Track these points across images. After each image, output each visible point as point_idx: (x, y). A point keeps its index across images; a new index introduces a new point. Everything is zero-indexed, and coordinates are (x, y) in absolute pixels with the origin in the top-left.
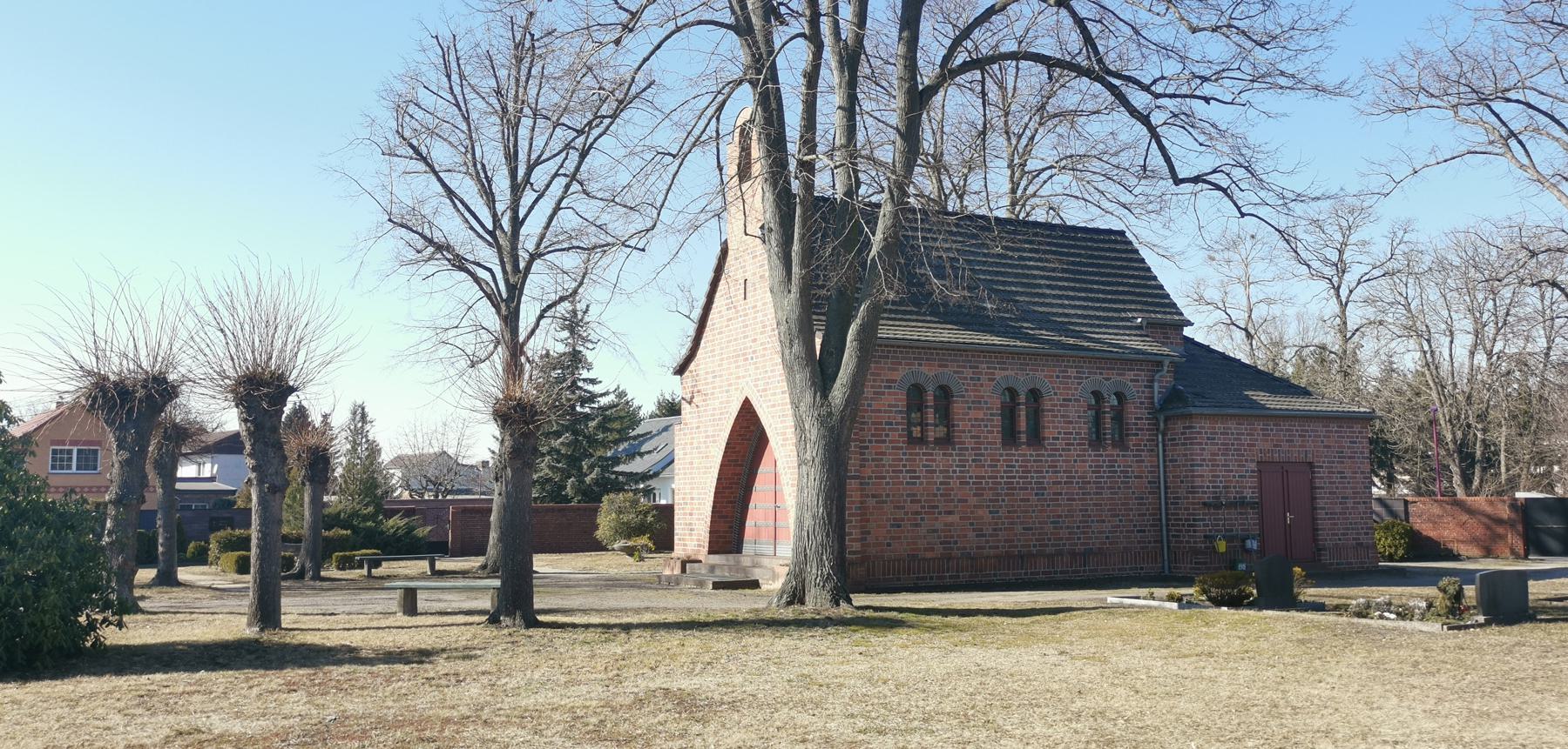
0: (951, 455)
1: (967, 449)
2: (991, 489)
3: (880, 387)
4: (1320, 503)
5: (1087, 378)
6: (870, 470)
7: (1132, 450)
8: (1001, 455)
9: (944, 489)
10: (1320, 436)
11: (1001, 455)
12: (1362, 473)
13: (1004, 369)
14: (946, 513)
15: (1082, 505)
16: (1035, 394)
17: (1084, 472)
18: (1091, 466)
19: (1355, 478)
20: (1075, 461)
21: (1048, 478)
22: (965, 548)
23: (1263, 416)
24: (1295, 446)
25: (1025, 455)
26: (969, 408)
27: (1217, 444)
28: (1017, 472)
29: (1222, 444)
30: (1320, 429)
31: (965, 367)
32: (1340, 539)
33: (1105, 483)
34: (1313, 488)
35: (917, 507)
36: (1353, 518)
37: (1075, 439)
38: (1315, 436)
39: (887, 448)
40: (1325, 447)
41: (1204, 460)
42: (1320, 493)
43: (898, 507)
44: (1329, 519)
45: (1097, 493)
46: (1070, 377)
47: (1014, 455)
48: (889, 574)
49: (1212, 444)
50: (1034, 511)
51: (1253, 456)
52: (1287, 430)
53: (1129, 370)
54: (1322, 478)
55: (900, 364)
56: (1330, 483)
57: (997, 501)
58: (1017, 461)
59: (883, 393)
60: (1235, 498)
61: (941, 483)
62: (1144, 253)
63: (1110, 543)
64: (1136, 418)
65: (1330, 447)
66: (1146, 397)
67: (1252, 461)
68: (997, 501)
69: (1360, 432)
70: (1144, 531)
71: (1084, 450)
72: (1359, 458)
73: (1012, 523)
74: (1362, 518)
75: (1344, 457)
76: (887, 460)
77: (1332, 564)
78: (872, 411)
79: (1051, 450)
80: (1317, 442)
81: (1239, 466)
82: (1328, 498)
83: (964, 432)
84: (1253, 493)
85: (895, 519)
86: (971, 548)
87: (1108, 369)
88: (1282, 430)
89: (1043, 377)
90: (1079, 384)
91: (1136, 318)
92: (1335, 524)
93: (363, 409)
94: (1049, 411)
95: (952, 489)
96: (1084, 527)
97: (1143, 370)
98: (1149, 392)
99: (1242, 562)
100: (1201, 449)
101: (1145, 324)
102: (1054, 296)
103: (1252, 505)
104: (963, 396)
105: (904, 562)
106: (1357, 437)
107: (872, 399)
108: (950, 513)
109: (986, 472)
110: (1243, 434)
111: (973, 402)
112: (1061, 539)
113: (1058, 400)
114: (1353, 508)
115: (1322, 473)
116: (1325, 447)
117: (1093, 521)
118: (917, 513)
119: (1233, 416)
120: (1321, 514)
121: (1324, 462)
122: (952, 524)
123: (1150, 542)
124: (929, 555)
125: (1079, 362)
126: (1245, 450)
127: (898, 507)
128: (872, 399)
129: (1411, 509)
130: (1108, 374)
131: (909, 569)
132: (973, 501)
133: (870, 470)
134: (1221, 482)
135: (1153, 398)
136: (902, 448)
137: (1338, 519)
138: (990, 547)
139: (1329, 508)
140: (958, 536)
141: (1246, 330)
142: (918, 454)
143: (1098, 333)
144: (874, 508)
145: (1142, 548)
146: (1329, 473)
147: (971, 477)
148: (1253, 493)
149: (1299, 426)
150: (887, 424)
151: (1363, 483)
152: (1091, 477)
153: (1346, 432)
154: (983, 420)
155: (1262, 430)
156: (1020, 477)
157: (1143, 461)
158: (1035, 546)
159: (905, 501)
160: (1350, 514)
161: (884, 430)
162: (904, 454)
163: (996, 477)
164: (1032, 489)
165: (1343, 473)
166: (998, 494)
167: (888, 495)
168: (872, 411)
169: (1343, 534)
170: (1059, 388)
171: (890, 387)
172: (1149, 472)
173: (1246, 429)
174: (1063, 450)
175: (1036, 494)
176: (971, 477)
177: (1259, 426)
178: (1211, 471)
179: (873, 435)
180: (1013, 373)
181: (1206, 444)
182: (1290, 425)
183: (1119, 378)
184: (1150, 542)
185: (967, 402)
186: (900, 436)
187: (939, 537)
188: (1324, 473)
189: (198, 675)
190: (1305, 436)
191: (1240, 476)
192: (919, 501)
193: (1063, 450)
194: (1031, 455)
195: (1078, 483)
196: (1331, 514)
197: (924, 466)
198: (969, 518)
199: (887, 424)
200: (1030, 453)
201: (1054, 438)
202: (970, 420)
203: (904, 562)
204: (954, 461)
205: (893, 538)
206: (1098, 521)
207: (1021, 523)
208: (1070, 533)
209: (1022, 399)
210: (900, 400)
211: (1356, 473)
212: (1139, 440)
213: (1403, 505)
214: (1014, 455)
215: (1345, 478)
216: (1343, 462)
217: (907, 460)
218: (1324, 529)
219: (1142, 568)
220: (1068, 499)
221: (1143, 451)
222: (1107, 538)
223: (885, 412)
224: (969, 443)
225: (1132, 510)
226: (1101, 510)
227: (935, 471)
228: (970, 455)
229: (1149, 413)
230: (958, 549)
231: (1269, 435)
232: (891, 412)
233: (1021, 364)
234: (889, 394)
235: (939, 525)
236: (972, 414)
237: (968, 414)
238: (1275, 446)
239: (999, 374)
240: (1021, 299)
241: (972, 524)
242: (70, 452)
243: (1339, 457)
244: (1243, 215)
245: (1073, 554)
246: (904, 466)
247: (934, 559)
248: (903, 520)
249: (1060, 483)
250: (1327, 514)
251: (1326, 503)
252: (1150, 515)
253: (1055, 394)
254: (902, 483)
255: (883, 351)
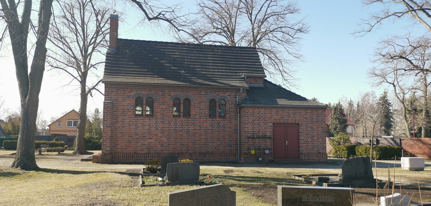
0: (152, 120)
1: (159, 118)
2: (167, 131)
3: (125, 98)
4: (301, 138)
5: (209, 95)
6: (120, 124)
7: (227, 119)
8: (172, 120)
9: (148, 131)
11: (172, 120)
13: (175, 92)
14: (149, 139)
15: (205, 137)
18: (209, 124)
20: (203, 122)
21: (191, 128)
22: (156, 150)
23: (276, 107)
24: (291, 118)
26: (160, 105)
27: (255, 117)
28: (179, 126)
30: (303, 112)
31: (159, 91)
32: (310, 151)
34: (299, 132)
35: (138, 137)
37: (203, 115)
39: (127, 117)
41: (249, 122)
43: (130, 137)
46: (202, 94)
47: (178, 120)
48: (125, 158)
49: (253, 117)
50: (185, 139)
51: (271, 121)
53: (227, 92)
55: (133, 90)
58: (179, 122)
59: (126, 100)
60: (262, 135)
61: (147, 129)
62: (28, 37)
63: (217, 150)
64: (229, 108)
65: (307, 118)
66: (234, 101)
67: (270, 123)
70: (232, 146)
71: (207, 119)
73: (176, 143)
74: (321, 143)
76: (127, 121)
78: (121, 106)
79: (193, 118)
82: (305, 136)
83: (158, 112)
84: (270, 134)
85: (128, 141)
86: (159, 150)
87: (218, 91)
89: (191, 95)
90: (206, 97)
91: (243, 75)
93: (98, 110)
94: (193, 105)
95: (152, 131)
96: (205, 144)
97: (233, 92)
98: (235, 99)
99: (260, 158)
100: (248, 118)
101: (245, 77)
102: (213, 69)
103: (270, 138)
104: (158, 101)
105: (131, 154)
107: (121, 102)
108: (151, 139)
109: (166, 125)
110: (267, 113)
111: (162, 103)
112: (196, 148)
113: (197, 102)
117: (209, 143)
118: (137, 139)
119: (262, 107)
120: (301, 142)
122: (151, 142)
123: (233, 150)
124: (142, 152)
125: (206, 89)
127: (130, 137)
128: (121, 102)
129: (402, 142)
130: (218, 93)
131: (133, 157)
132: (160, 135)
133: (120, 124)
134: (256, 130)
135: (236, 101)
136: (132, 118)
138: (166, 150)
139: (305, 140)
140: (154, 146)
141: (393, 84)
142: (139, 120)
143: (220, 80)
144: (120, 137)
145: (230, 152)
147: (160, 127)
149: (293, 110)
150: (127, 110)
151: (322, 131)
153: (314, 113)
154: (165, 108)
156: (179, 127)
157: (232, 123)
158: (185, 150)
159: (133, 135)
161: (126, 111)
162: (133, 119)
163: (170, 127)
164: (185, 131)
166: (170, 133)
167: (126, 133)
168: (121, 106)
170: (197, 98)
171: (129, 98)
172: (234, 126)
175: (186, 133)
176: (160, 127)
177: (274, 111)
179: (121, 113)
180: (178, 93)
181: (250, 117)
183: (223, 95)
184: (233, 150)
185: (159, 103)
186: (132, 113)
187: (146, 147)
188: (303, 127)
192: (139, 135)
194: (185, 120)
195: (204, 130)
197: (141, 123)
198: (158, 141)
199: (127, 110)
200: (184, 119)
201: (194, 115)
202: (160, 108)
203: (131, 154)
204: (153, 122)
205: (127, 146)
207: (180, 143)
208: (199, 146)
209: (182, 102)
210: (133, 102)
212: (231, 115)
213: (399, 140)
214: (178, 120)
217: (134, 121)
219: (229, 159)
220: (199, 135)
221: (232, 119)
222: (215, 148)
223: (126, 106)
224: (159, 116)
225: (226, 139)
226: (213, 139)
227: (145, 125)
228: (160, 120)
229: (235, 106)
230: (153, 150)
232: (129, 106)
233: (182, 90)
234: (128, 100)
235: (145, 143)
236: (161, 107)
237: (160, 106)
239: (173, 94)
240: (198, 70)
241: (159, 143)
242: (72, 122)
244: (179, 30)
245: (200, 153)
246: (133, 123)
247: (143, 154)
248: (132, 141)
252: (234, 141)
253: (196, 100)
254: (132, 129)
255: (126, 86)
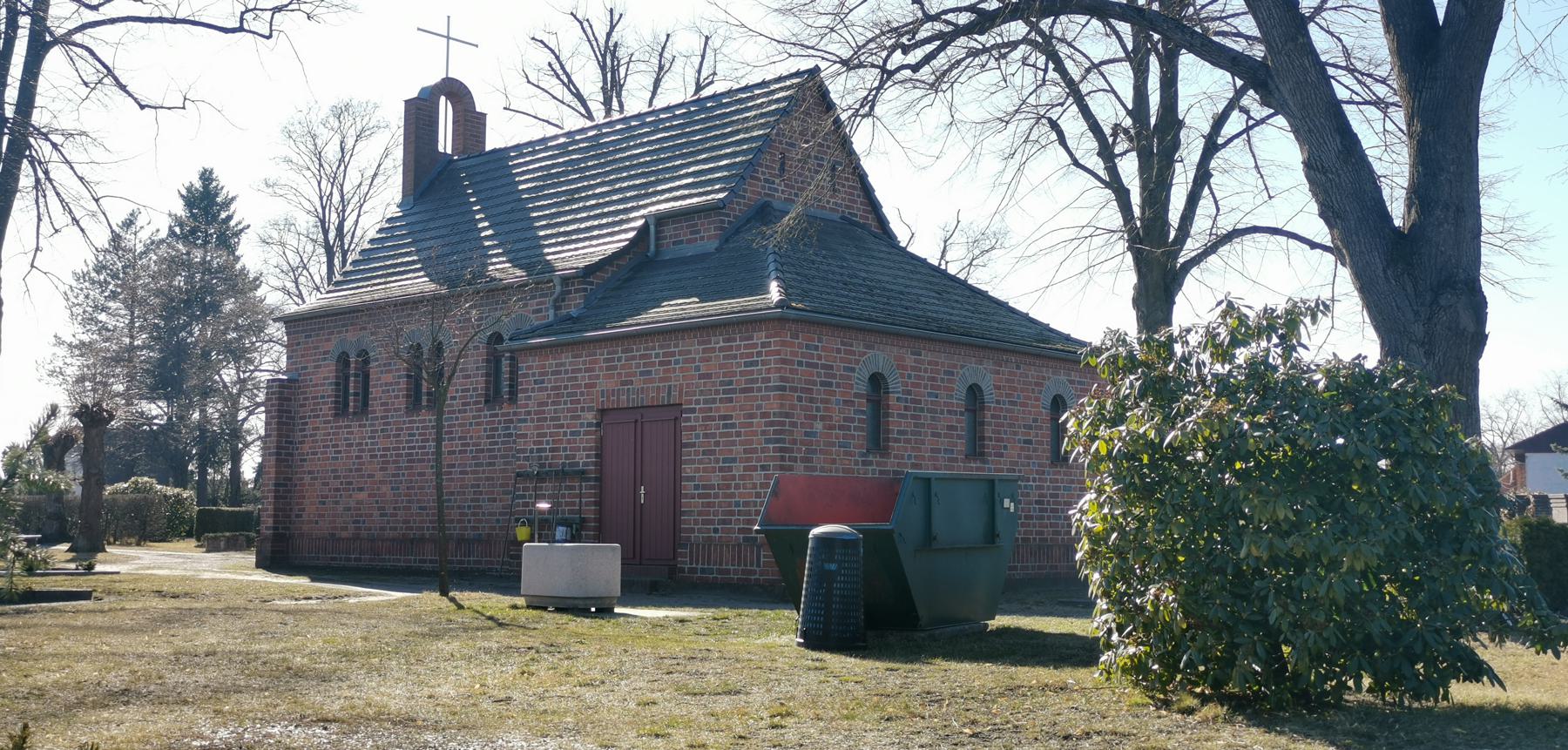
4: (688, 470)
10: (694, 360)
12: (764, 415)
16: (363, 353)
17: (479, 438)
19: (751, 425)
25: (424, 421)
29: (553, 388)
30: (695, 347)
32: (716, 530)
33: (499, 450)
36: (741, 495)
38: (686, 361)
40: (701, 377)
41: (529, 413)
42: (689, 454)
44: (700, 496)
45: (490, 464)
49: (541, 389)
52: (642, 357)
54: (693, 428)
56: (706, 436)
57: (398, 475)
67: (590, 409)
68: (398, 475)
69: (764, 345)
72: (760, 390)
75: (733, 391)
76: (320, 435)
77: (693, 571)
80: (688, 370)
81: (573, 418)
84: (588, 456)
88: (633, 358)
92: (709, 505)
96: (474, 507)
106: (759, 354)
108: (361, 489)
114: (742, 477)
115: (693, 420)
116: (701, 377)
120: (688, 487)
121: (698, 402)
124: (344, 534)
126: (582, 394)
132: (379, 476)
136: (329, 422)
137: (716, 496)
139: (701, 478)
142: (341, 427)
146: (705, 419)
148: (588, 456)
149: (661, 347)
152: (485, 443)
154: (391, 384)
155: (606, 360)
160: (737, 487)
165: (730, 417)
169: (724, 522)
173: (584, 363)
174: (459, 411)
178: (538, 428)
182: (646, 349)
188: (696, 419)
189: (963, 665)
190: (669, 363)
191: (572, 433)
193: (459, 411)
196: (704, 487)
206: (489, 500)
211: (751, 416)
215: (733, 426)
216: (731, 400)
218: (690, 513)
231: (615, 368)
238: (623, 383)
241: (377, 502)
243: (725, 392)
249: (454, 452)
250: (697, 487)
251: (697, 470)
